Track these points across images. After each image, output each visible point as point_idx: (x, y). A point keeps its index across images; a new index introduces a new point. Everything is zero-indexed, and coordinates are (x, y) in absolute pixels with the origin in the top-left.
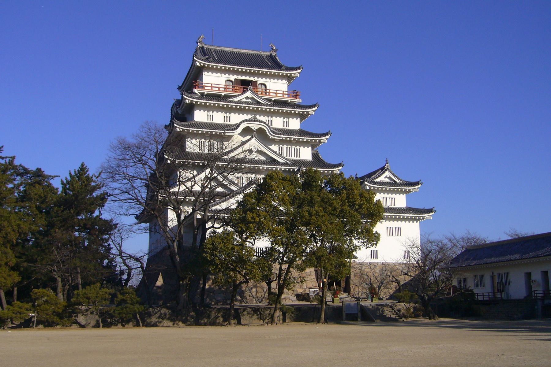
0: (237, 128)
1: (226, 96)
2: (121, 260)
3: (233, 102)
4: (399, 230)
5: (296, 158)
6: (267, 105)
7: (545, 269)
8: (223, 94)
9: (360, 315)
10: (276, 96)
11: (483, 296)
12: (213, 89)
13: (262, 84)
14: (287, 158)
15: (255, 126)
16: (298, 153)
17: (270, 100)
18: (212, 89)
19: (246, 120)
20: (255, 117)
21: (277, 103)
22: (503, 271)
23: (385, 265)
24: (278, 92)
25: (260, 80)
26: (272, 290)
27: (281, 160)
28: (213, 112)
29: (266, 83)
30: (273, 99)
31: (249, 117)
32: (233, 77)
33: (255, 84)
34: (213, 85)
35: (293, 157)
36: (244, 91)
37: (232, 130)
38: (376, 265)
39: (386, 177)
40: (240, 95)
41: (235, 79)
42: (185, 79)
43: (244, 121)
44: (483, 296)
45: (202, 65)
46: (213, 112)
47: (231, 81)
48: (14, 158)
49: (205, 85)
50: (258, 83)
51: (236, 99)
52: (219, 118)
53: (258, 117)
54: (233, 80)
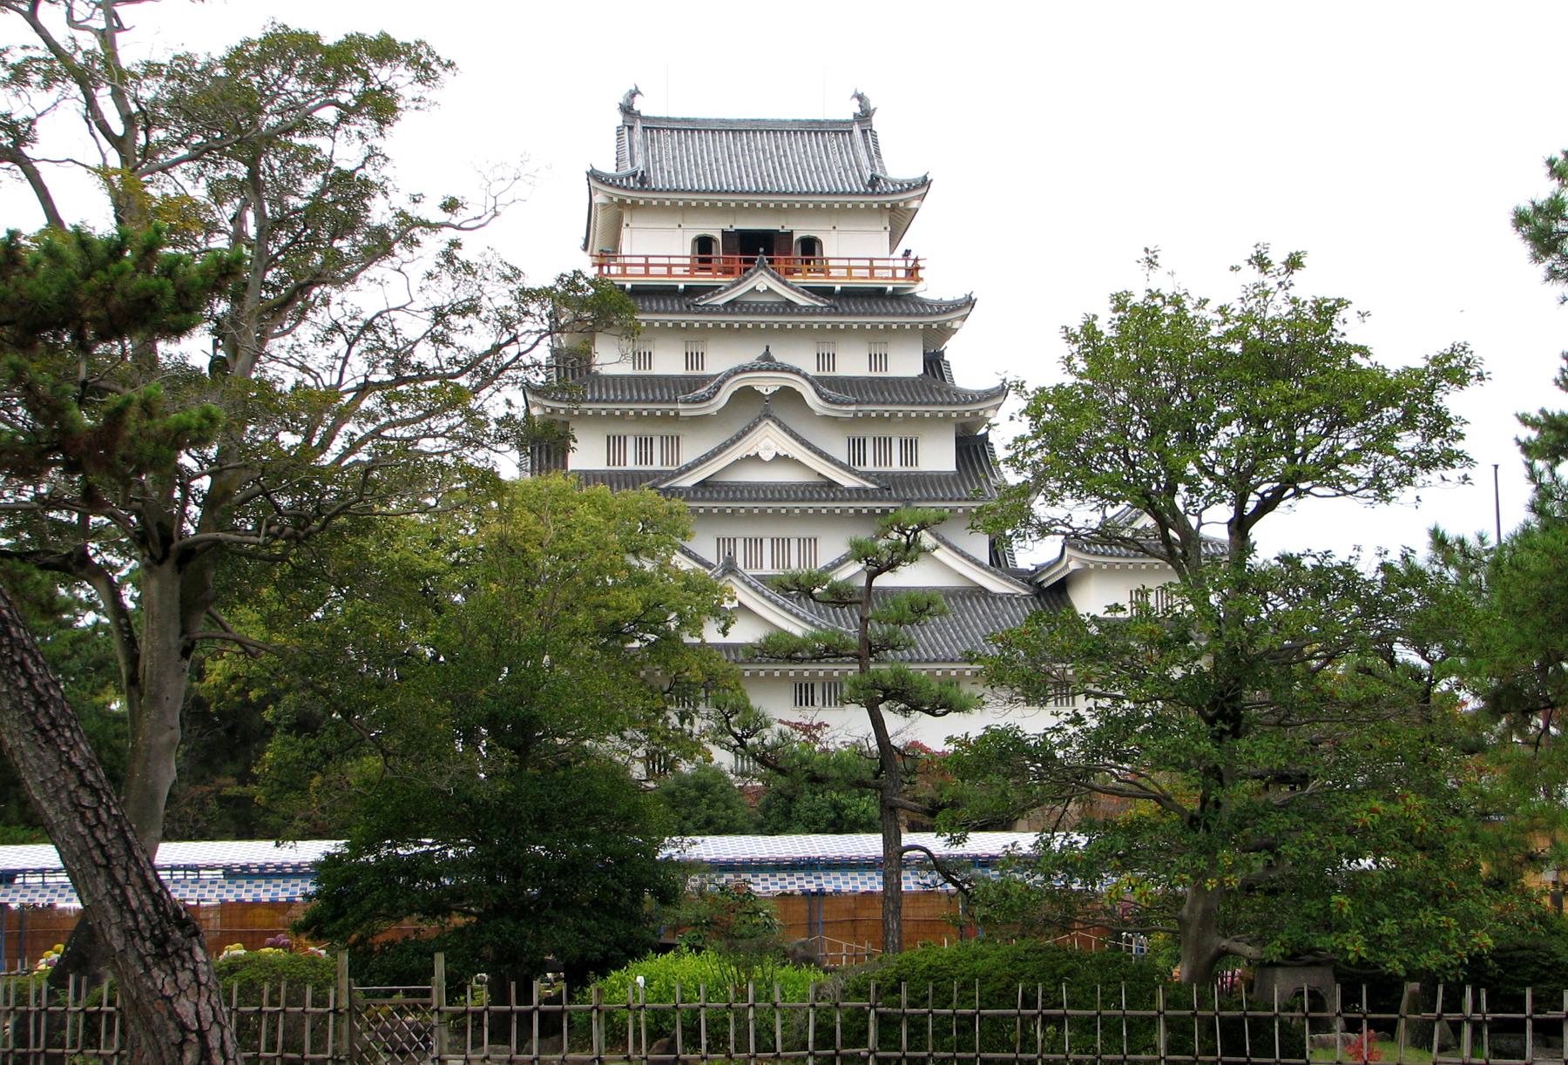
0: (715, 394)
1: (691, 291)
2: (281, 367)
3: (714, 310)
5: (904, 469)
8: (890, 288)
10: (850, 276)
12: (652, 270)
15: (767, 384)
16: (909, 447)
17: (825, 292)
18: (647, 274)
19: (743, 370)
20: (767, 357)
24: (853, 263)
25: (801, 230)
27: (847, 481)
31: (748, 354)
34: (651, 261)
36: (746, 270)
37: (701, 401)
40: (739, 283)
41: (723, 232)
42: (735, 129)
43: (735, 372)
48: (593, 175)
49: (831, 263)
50: (796, 237)
51: (721, 300)
52: (668, 362)
53: (780, 356)
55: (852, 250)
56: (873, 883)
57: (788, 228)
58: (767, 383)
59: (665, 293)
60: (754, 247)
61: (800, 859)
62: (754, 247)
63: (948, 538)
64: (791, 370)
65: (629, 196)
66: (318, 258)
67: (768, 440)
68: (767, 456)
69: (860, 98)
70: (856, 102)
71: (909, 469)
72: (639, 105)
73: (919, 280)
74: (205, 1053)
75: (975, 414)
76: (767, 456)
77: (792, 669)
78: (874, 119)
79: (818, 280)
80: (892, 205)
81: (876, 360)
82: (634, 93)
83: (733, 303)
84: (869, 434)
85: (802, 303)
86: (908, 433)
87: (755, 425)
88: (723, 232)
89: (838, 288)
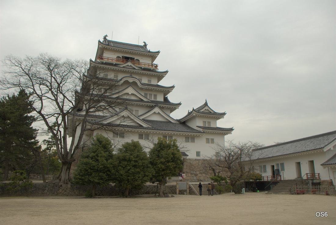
1: (116, 65)
3: (121, 67)
4: (212, 140)
6: (139, 70)
7: (311, 160)
9: (188, 191)
11: (267, 178)
12: (109, 60)
13: (137, 60)
14: (150, 99)
15: (131, 80)
16: (155, 96)
17: (141, 68)
21: (145, 69)
22: (279, 162)
23: (204, 160)
25: (136, 58)
26: (10, 97)
27: (145, 100)
28: (155, 144)
29: (139, 60)
30: (143, 68)
31: (128, 75)
32: (121, 55)
33: (132, 59)
35: (153, 99)
38: (198, 160)
39: (206, 109)
41: (122, 56)
43: (123, 78)
44: (267, 178)
45: (103, 47)
46: (155, 144)
47: (120, 57)
48: (99, 41)
49: (104, 58)
50: (135, 59)
51: (122, 66)
54: (121, 57)
55: (145, 62)
56: (267, 180)
57: (134, 57)
58: (131, 80)
59: (111, 64)
60: (127, 59)
61: (20, 196)
62: (127, 59)
63: (164, 112)
64: (135, 78)
65: (106, 46)
66: (6, 128)
67: (130, 90)
68: (130, 93)
69: (145, 43)
70: (144, 43)
71: (155, 100)
72: (107, 38)
73: (157, 68)
74: (1, 89)
75: (168, 91)
76: (130, 93)
77: (136, 130)
78: (147, 46)
79: (140, 66)
80: (153, 55)
81: (149, 81)
82: (106, 36)
83: (123, 67)
84: (148, 93)
85: (137, 69)
86: (155, 93)
87: (128, 87)
88: (122, 56)
89: (143, 68)
